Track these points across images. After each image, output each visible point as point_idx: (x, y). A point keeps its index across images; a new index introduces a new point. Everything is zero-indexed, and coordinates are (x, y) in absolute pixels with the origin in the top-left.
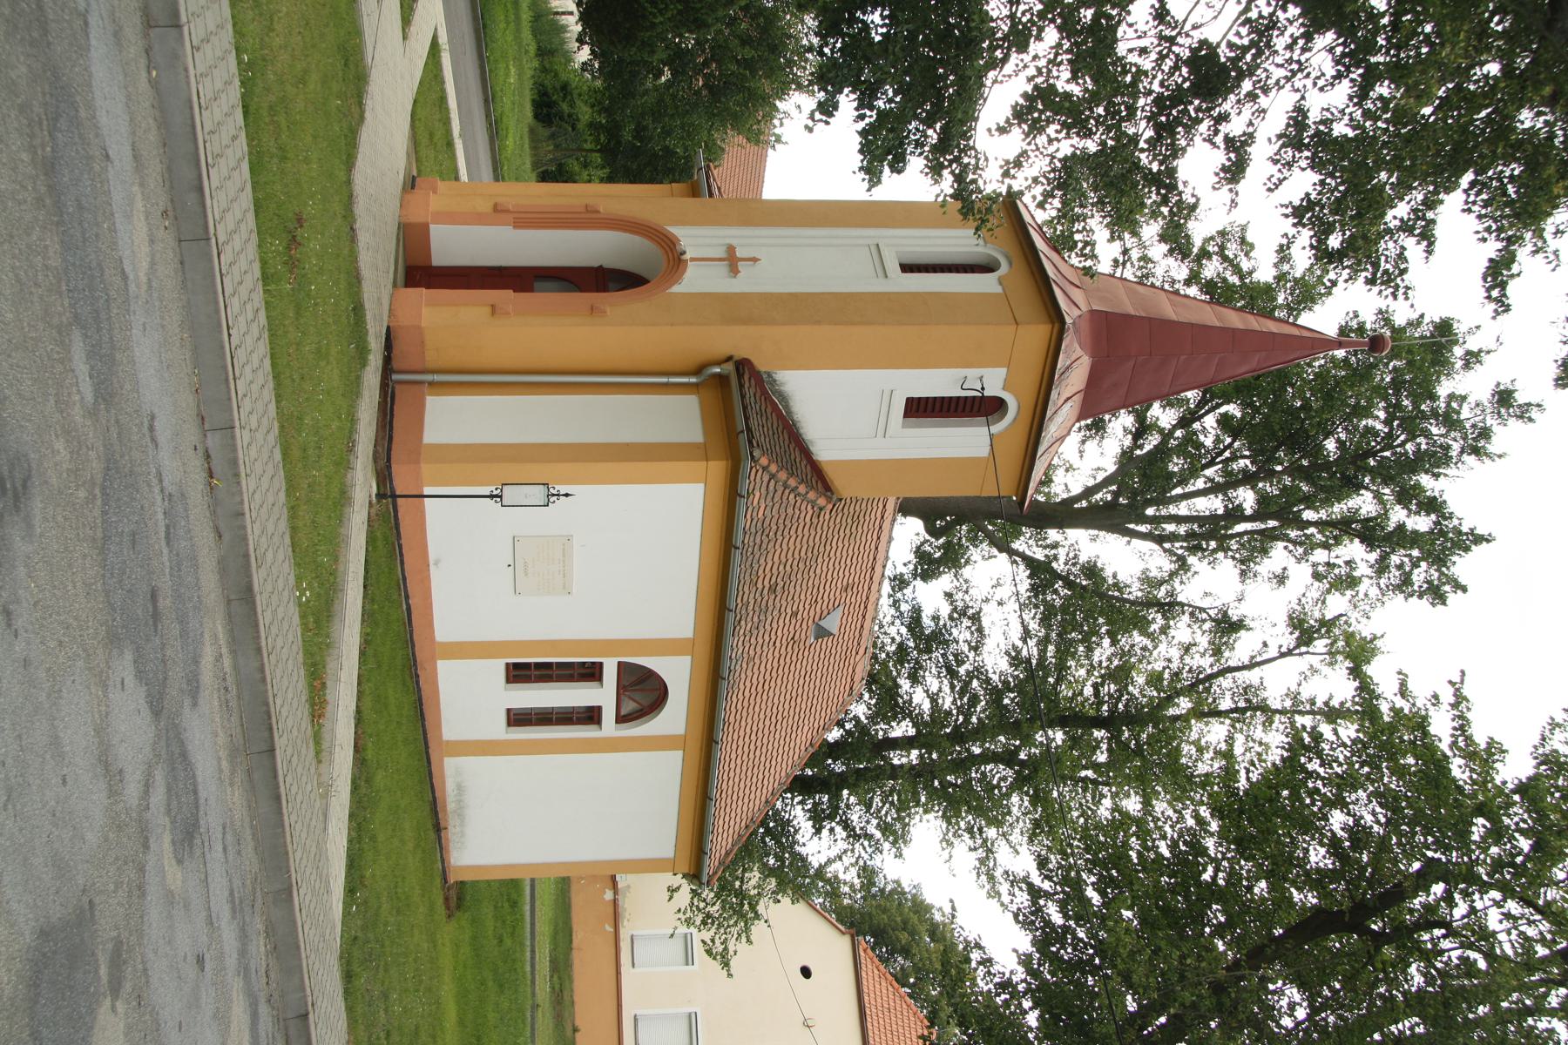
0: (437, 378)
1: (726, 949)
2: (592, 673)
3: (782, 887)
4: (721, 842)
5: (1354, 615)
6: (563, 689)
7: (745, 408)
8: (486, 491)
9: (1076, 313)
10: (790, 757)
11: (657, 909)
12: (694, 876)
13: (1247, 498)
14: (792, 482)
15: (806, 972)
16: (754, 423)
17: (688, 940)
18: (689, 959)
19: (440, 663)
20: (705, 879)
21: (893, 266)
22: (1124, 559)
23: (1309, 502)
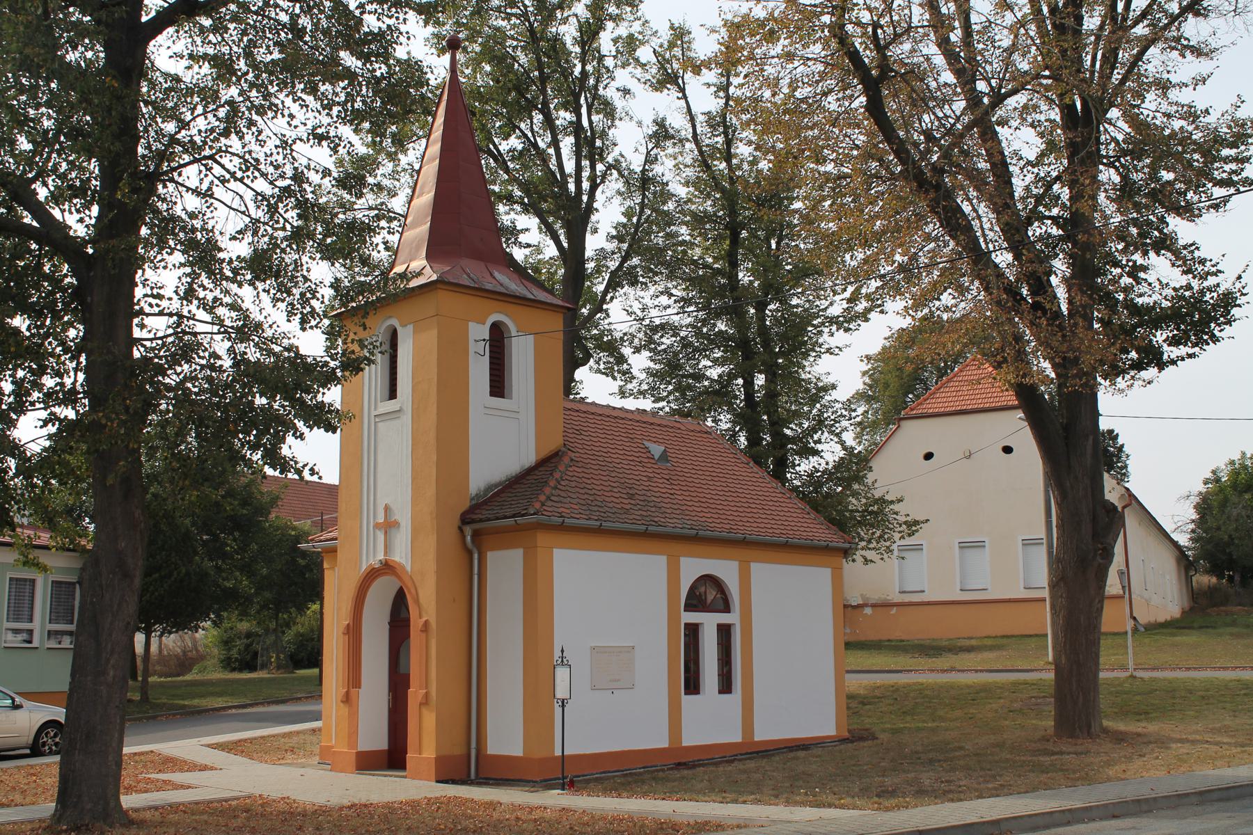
0: (473, 745)
1: (905, 523)
2: (693, 631)
3: (859, 479)
4: (822, 533)
5: (655, 42)
6: (705, 653)
7: (498, 519)
8: (558, 710)
9: (428, 270)
10: (757, 479)
11: (876, 575)
12: (846, 553)
13: (564, 117)
14: (552, 483)
15: (929, 456)
16: (509, 512)
17: (903, 549)
18: (918, 548)
19: (684, 744)
20: (847, 545)
21: (392, 405)
22: (609, 212)
23: (566, 73)
